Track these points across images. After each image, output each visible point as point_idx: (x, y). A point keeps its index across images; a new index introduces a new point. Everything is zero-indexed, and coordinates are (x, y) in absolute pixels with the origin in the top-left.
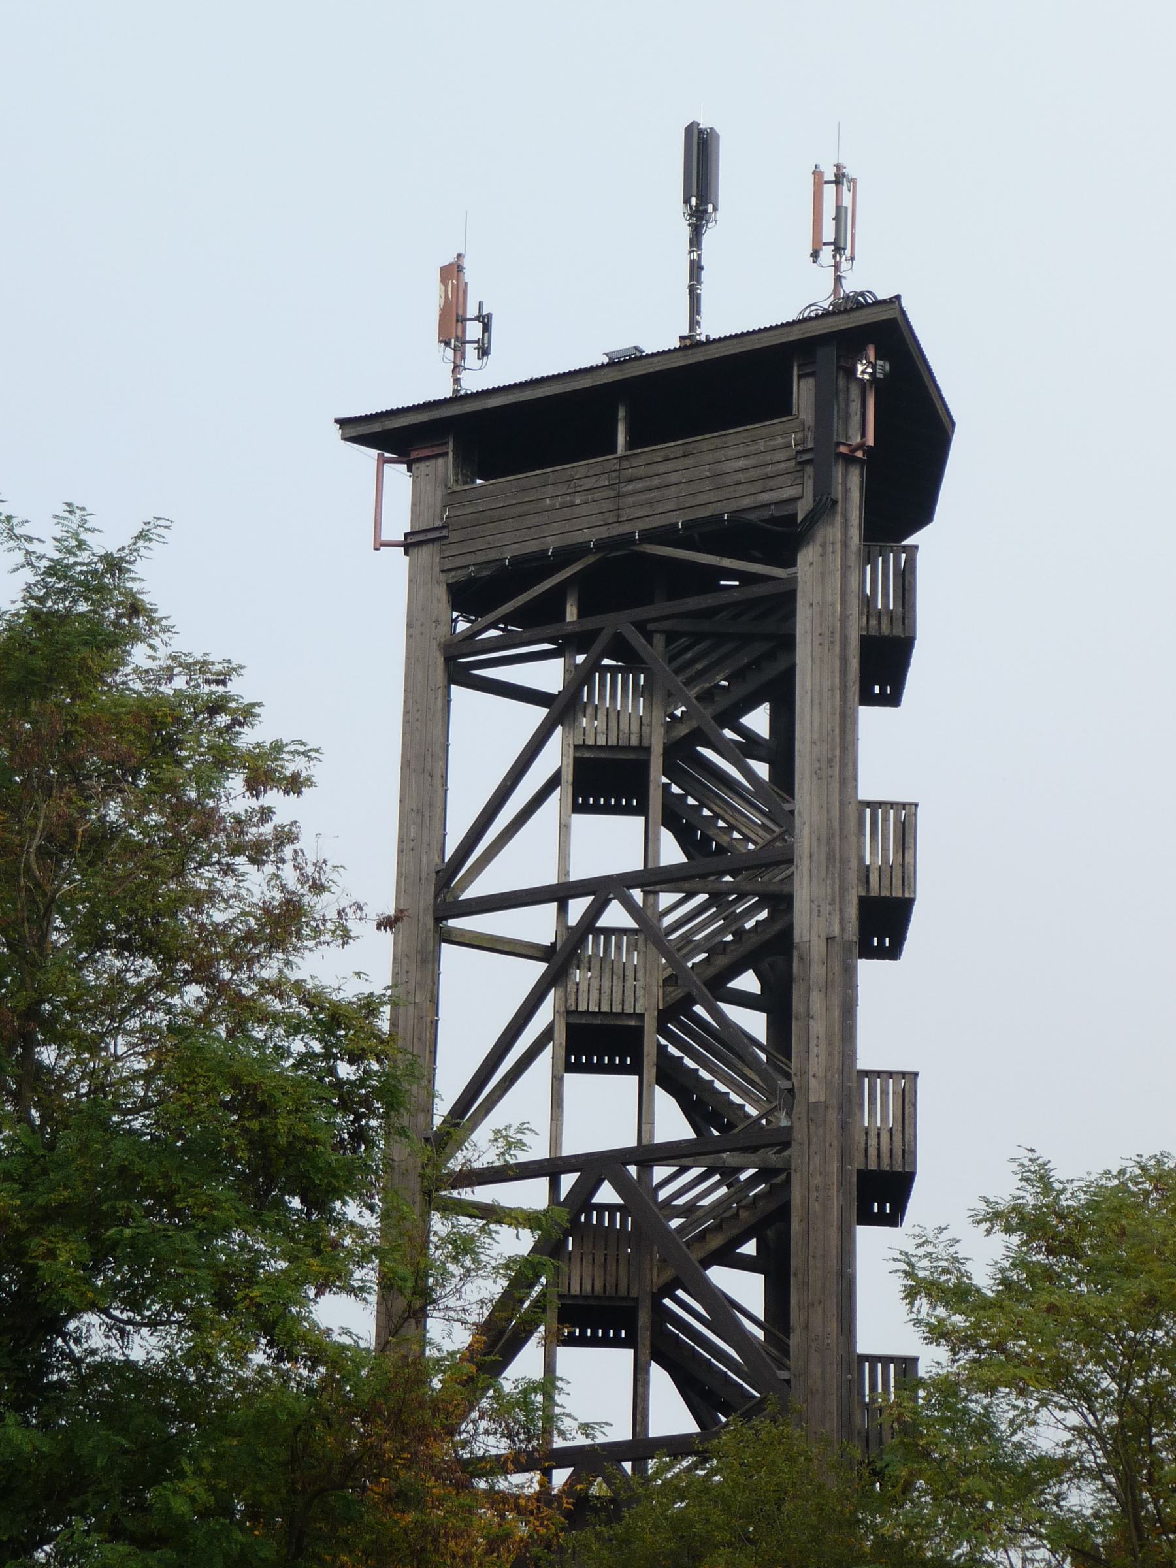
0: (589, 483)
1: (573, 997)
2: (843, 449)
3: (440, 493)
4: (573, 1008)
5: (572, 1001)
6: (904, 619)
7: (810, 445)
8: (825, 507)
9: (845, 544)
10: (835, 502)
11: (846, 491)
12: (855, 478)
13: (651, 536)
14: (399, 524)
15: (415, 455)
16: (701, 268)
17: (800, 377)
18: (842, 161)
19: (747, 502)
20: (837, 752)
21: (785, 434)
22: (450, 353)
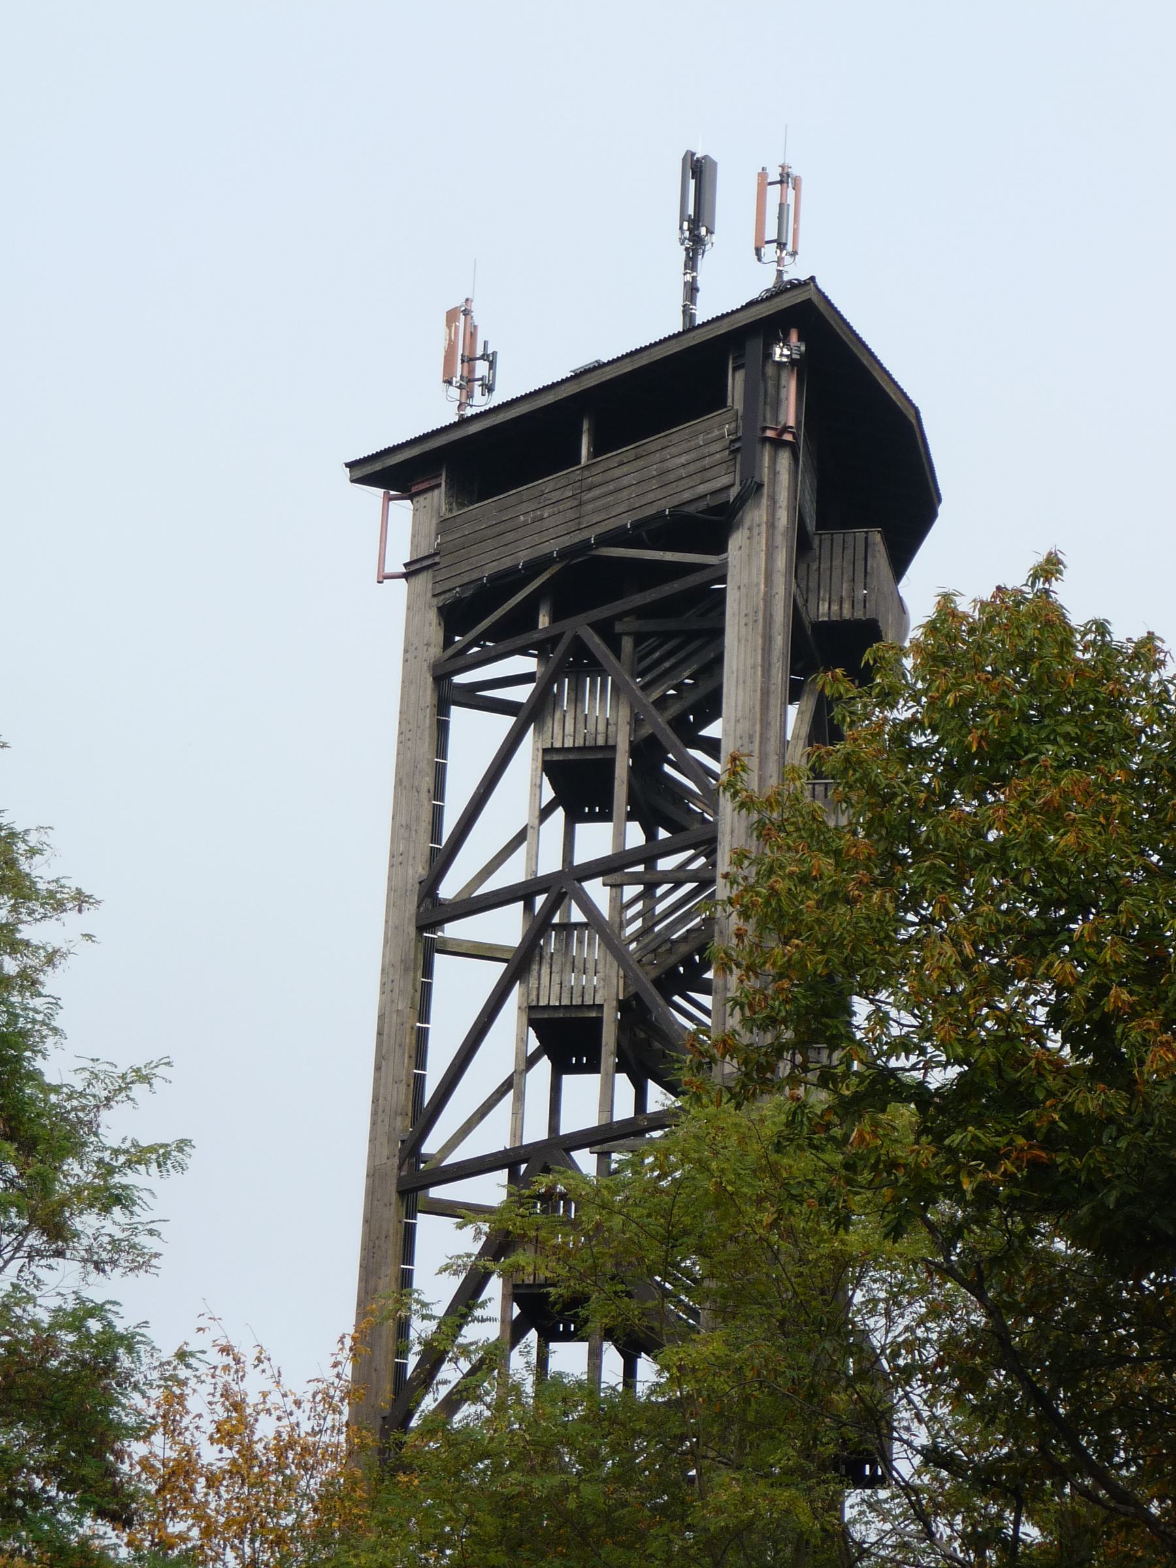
0: (556, 496)
1: (535, 993)
2: (770, 434)
3: (434, 522)
4: (534, 1003)
5: (533, 996)
6: (865, 602)
7: (740, 434)
8: (752, 490)
9: (772, 525)
10: (760, 486)
11: (774, 473)
12: (784, 460)
13: (610, 539)
14: (400, 555)
15: (414, 490)
16: (697, 290)
17: (735, 369)
18: (788, 162)
19: (687, 496)
20: (758, 727)
21: (721, 426)
22: (455, 392)
